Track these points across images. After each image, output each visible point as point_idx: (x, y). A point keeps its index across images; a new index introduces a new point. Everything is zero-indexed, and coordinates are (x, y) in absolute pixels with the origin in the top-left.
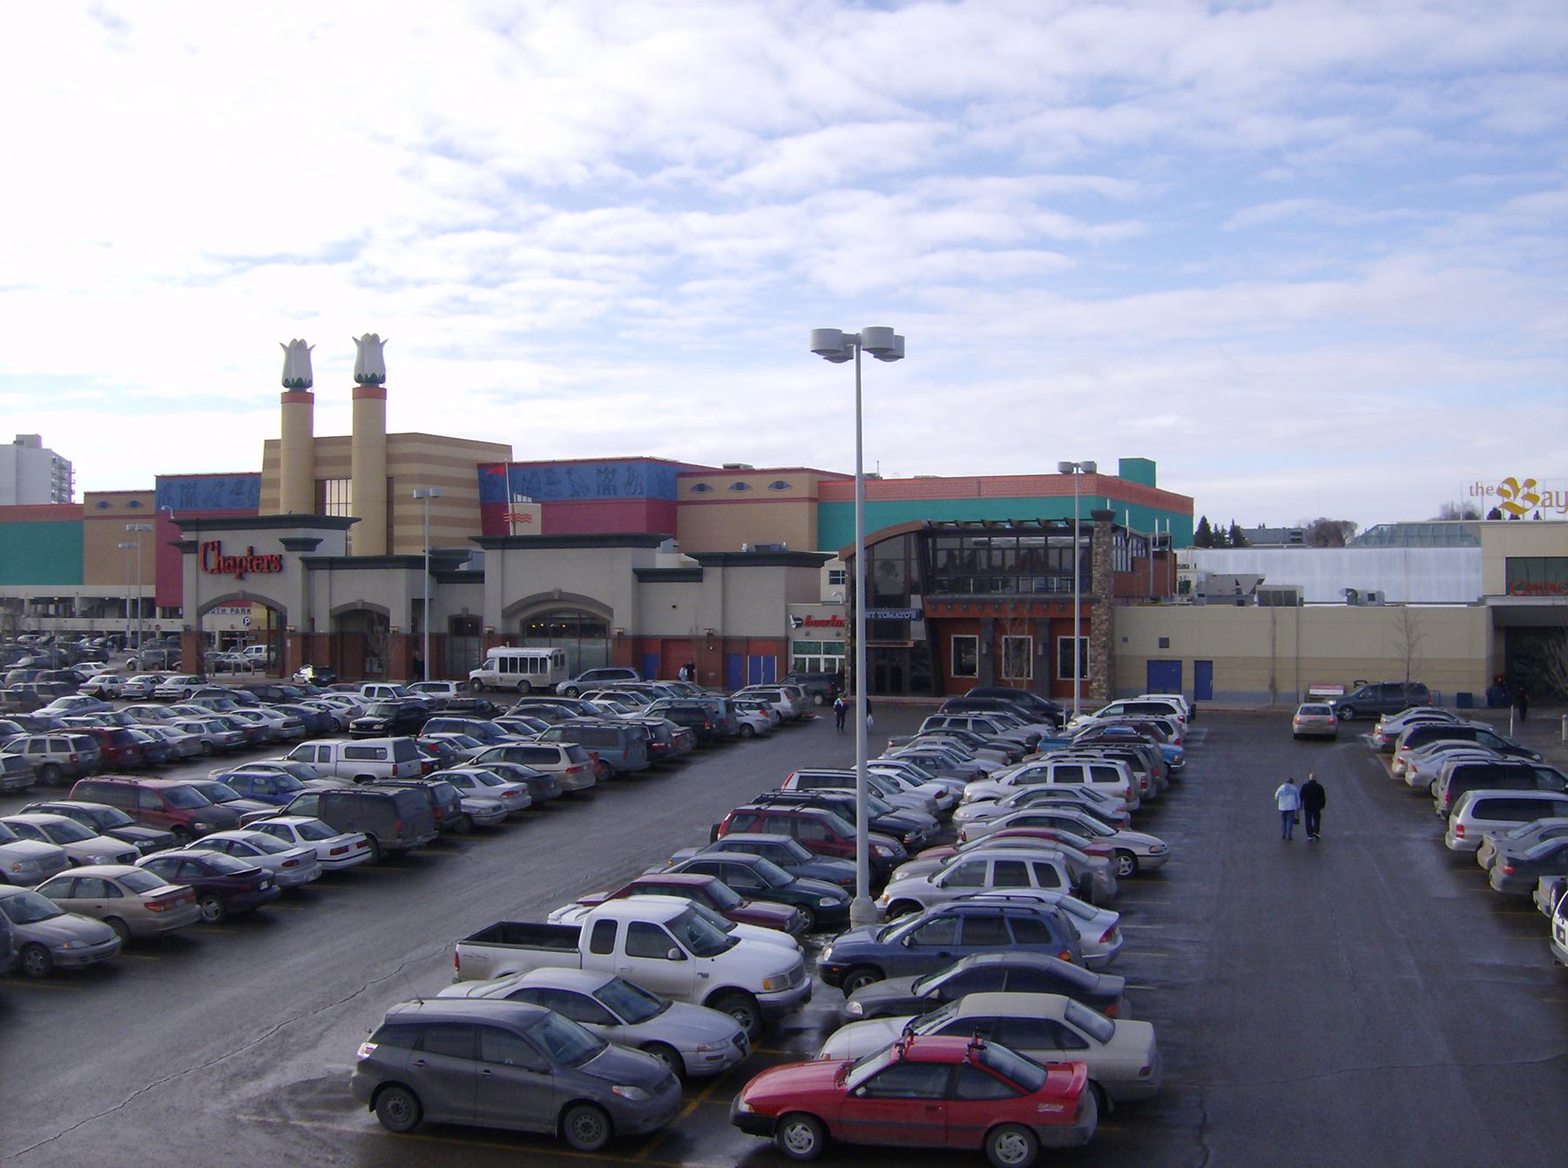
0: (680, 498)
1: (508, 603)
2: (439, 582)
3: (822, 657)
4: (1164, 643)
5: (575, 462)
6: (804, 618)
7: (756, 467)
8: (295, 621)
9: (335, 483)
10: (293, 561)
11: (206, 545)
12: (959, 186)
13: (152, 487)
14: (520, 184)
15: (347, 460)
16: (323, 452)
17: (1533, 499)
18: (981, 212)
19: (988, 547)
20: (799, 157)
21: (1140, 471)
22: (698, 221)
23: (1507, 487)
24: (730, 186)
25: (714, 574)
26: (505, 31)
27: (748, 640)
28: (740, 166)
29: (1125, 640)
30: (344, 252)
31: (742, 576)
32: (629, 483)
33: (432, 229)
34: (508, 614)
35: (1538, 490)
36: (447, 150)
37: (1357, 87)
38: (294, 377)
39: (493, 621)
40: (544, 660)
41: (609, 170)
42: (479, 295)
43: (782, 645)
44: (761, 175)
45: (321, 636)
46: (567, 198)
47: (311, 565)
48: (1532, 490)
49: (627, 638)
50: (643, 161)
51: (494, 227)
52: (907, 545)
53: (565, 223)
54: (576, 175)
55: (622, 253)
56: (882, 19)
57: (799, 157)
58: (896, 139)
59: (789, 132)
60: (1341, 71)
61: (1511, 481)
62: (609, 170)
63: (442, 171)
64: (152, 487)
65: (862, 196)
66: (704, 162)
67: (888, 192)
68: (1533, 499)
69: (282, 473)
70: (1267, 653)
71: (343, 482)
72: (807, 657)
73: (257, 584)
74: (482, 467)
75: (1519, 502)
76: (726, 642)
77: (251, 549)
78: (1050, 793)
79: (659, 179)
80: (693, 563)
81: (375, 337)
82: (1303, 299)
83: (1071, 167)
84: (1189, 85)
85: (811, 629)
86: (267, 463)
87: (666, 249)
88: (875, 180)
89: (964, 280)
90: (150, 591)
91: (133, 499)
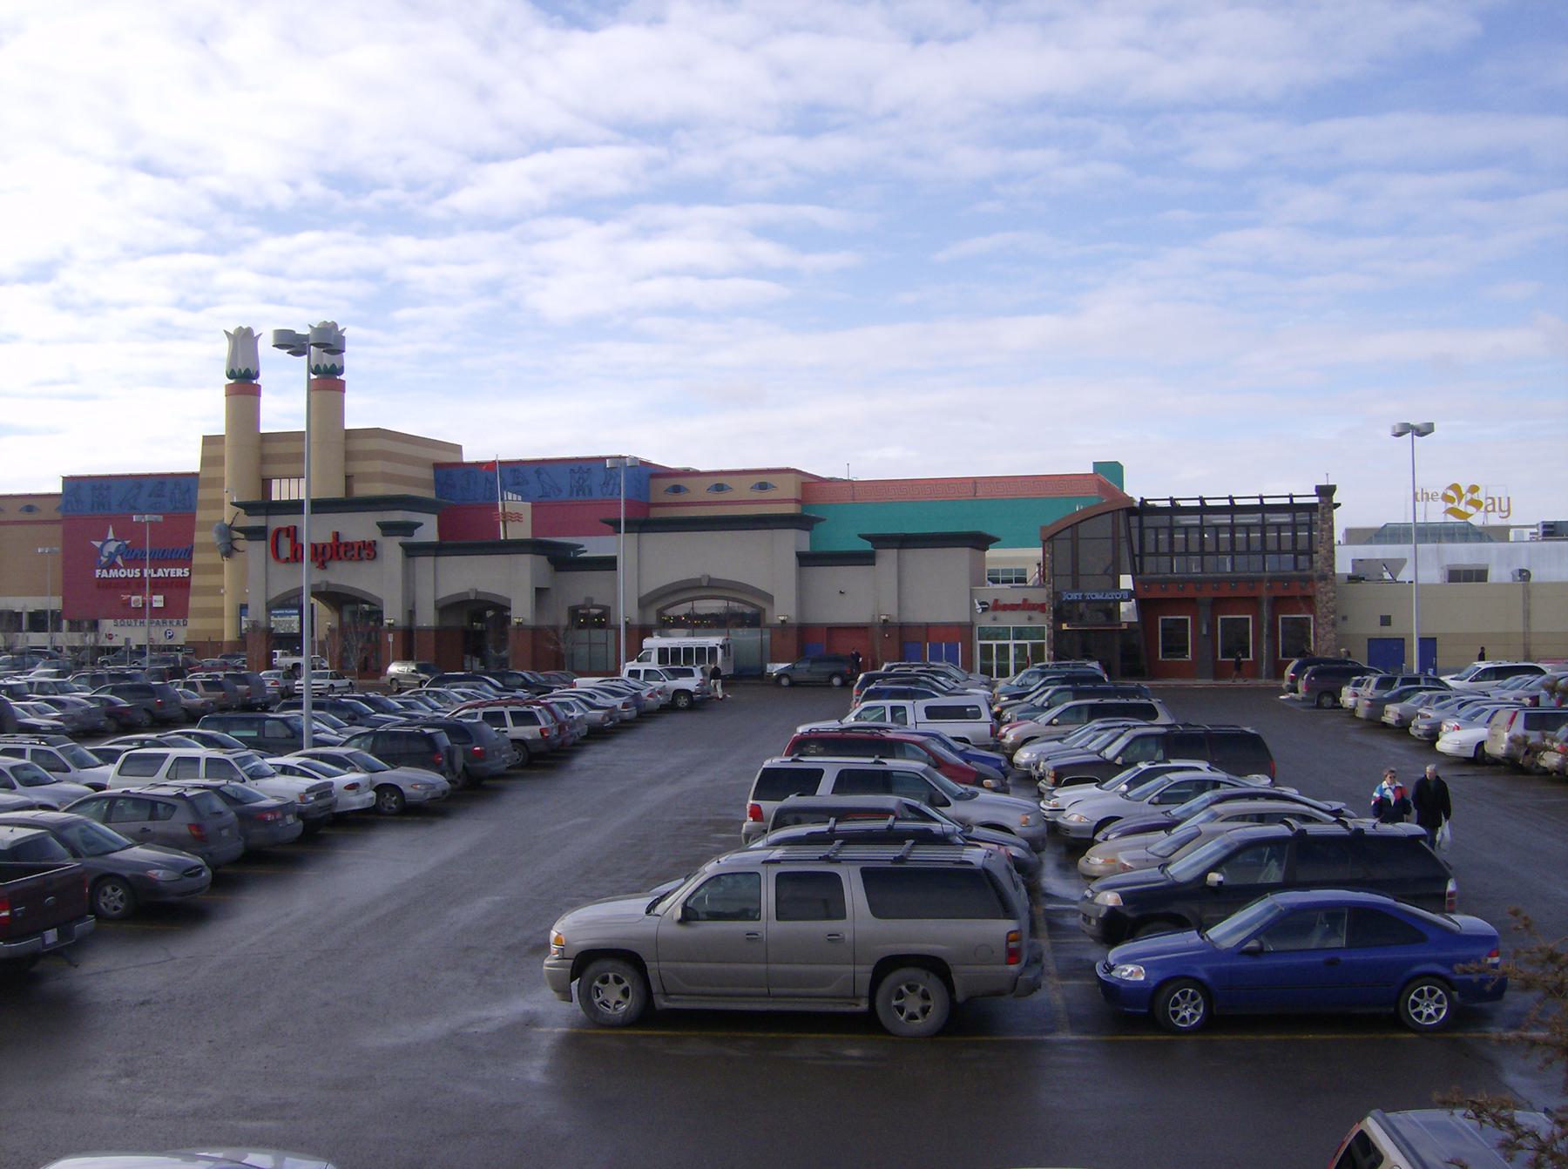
0: (652, 500)
1: (645, 592)
2: (557, 569)
3: (1011, 643)
4: (1386, 621)
5: (577, 459)
6: (991, 602)
7: (701, 469)
8: (393, 615)
9: (285, 482)
10: (391, 548)
11: (278, 531)
12: (670, 213)
13: (58, 489)
14: (227, 204)
15: (298, 458)
16: (271, 449)
17: (1476, 504)
18: (693, 241)
19: (1172, 529)
20: (506, 184)
21: (1110, 472)
22: (405, 246)
23: (1450, 493)
24: (437, 211)
25: (888, 557)
26: (203, 41)
27: (928, 628)
28: (451, 186)
29: (1345, 618)
30: (41, 272)
31: (919, 559)
32: (606, 484)
33: (133, 251)
34: (644, 603)
35: (1480, 496)
36: (145, 166)
37: (1066, 118)
38: (241, 367)
39: (625, 611)
40: (713, 651)
41: (313, 189)
42: (182, 318)
43: (964, 631)
44: (465, 199)
45: (427, 630)
46: (279, 221)
47: (411, 551)
48: (1475, 496)
49: (791, 626)
50: (348, 182)
51: (201, 249)
52: (1115, 525)
53: (273, 246)
54: (281, 196)
55: (333, 277)
56: (579, 37)
57: (506, 184)
58: (602, 165)
59: (498, 158)
60: (1045, 103)
61: (1455, 487)
62: (313, 189)
63: (144, 188)
64: (58, 489)
65: (573, 223)
66: (413, 185)
67: (599, 220)
68: (1476, 504)
69: (227, 472)
70: (1518, 627)
71: (294, 482)
72: (994, 643)
73: (344, 575)
74: (438, 466)
75: (1462, 507)
76: (903, 628)
77: (336, 535)
78: (820, 813)
79: (368, 202)
80: (867, 546)
81: (249, 331)
82: (1022, 333)
83: (781, 196)
84: (893, 115)
85: (1000, 614)
86: (206, 461)
87: (373, 275)
88: (586, 206)
89: (682, 310)
90: (54, 603)
91: (29, 503)
